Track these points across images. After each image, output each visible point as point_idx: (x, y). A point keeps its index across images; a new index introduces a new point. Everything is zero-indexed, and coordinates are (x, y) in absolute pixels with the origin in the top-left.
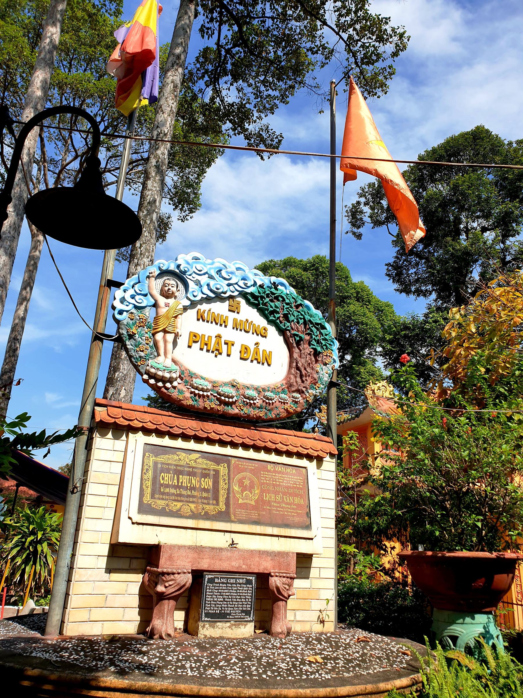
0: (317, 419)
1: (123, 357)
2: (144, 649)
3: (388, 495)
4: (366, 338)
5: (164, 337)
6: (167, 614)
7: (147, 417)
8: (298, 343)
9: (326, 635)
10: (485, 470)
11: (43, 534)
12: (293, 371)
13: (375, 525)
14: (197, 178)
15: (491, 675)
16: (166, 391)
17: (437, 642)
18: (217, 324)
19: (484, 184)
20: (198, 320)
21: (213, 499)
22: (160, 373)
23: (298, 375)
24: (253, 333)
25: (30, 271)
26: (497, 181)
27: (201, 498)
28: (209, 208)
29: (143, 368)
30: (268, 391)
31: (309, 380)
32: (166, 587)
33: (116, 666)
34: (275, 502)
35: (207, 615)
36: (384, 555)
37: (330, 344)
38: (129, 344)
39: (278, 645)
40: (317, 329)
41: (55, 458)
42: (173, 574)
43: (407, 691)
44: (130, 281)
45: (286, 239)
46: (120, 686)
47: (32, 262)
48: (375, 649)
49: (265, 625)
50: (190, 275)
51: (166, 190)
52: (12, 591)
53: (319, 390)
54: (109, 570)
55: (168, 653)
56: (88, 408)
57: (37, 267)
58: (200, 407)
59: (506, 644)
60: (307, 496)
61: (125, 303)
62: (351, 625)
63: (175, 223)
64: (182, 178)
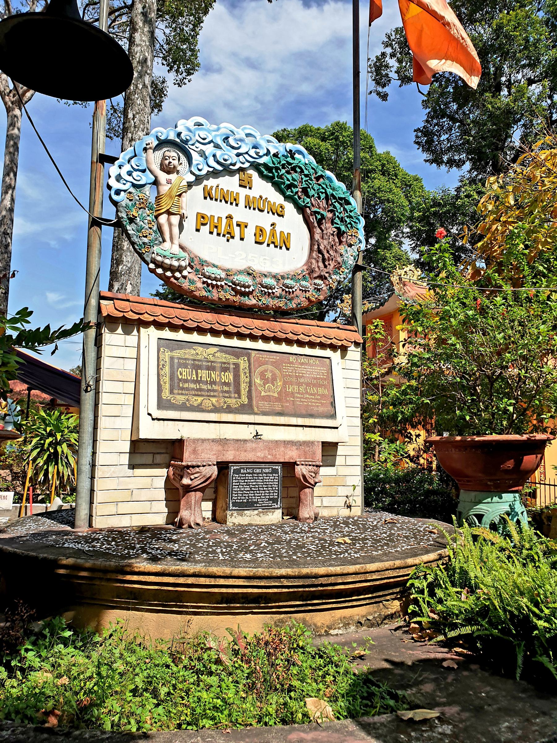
0: (339, 310)
1: (125, 248)
2: (174, 537)
3: (414, 383)
4: (392, 218)
5: (168, 220)
6: (195, 505)
7: (158, 311)
8: (320, 223)
9: (353, 518)
10: (519, 352)
11: (62, 436)
12: (314, 254)
13: (399, 414)
14: (193, 30)
15: (514, 547)
16: (176, 281)
17: (464, 520)
18: (226, 202)
19: (532, 24)
20: (205, 198)
21: (235, 393)
22: (167, 261)
23: (320, 259)
24: (268, 212)
25: (10, 153)
26: (548, 19)
27: (223, 392)
28: (209, 69)
29: (148, 256)
30: (288, 278)
31: (332, 264)
32: (191, 480)
33: (148, 553)
34: (299, 393)
35: (234, 504)
36: (409, 442)
37: (355, 222)
38: (130, 228)
39: (307, 529)
40: (341, 205)
41: (63, 357)
42: (198, 466)
43: (434, 565)
44: (125, 155)
45: (300, 104)
46: (154, 571)
47: (12, 143)
48: (403, 529)
49: (292, 512)
50: (193, 145)
51: (158, 46)
52: (38, 490)
53: (344, 276)
54: (132, 466)
55: (198, 541)
56: (93, 302)
57: (18, 148)
58: (215, 298)
59: (530, 519)
60: (331, 386)
61: (122, 181)
62: (377, 509)
63: (171, 89)
64: (175, 30)
